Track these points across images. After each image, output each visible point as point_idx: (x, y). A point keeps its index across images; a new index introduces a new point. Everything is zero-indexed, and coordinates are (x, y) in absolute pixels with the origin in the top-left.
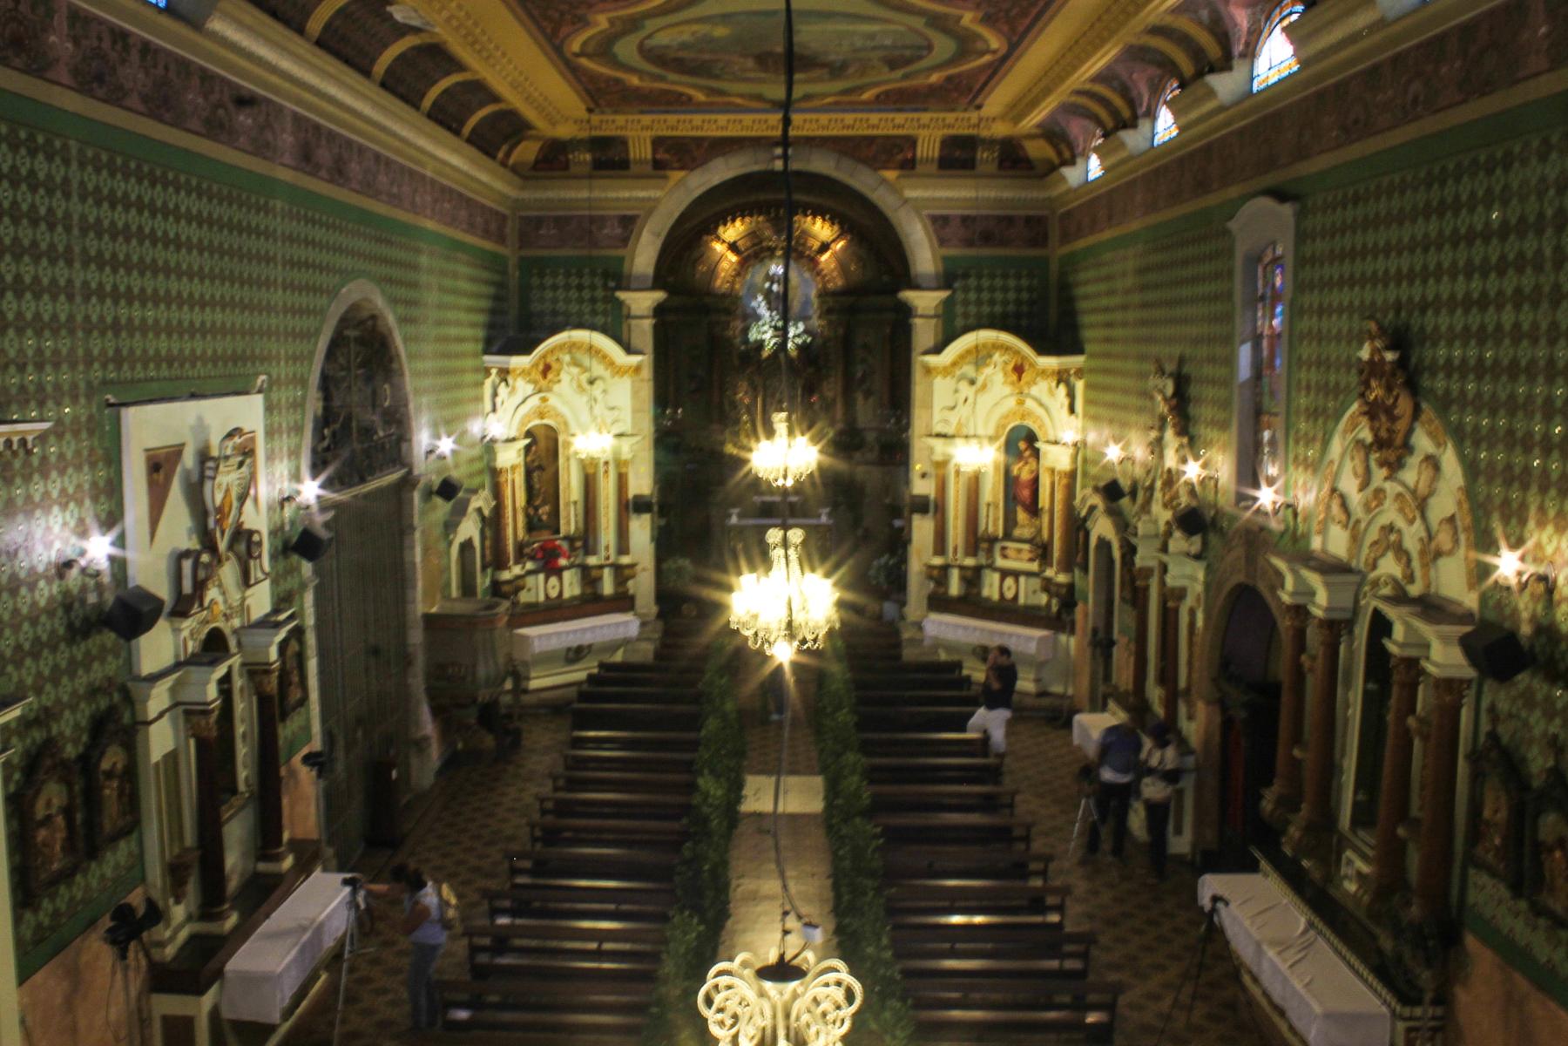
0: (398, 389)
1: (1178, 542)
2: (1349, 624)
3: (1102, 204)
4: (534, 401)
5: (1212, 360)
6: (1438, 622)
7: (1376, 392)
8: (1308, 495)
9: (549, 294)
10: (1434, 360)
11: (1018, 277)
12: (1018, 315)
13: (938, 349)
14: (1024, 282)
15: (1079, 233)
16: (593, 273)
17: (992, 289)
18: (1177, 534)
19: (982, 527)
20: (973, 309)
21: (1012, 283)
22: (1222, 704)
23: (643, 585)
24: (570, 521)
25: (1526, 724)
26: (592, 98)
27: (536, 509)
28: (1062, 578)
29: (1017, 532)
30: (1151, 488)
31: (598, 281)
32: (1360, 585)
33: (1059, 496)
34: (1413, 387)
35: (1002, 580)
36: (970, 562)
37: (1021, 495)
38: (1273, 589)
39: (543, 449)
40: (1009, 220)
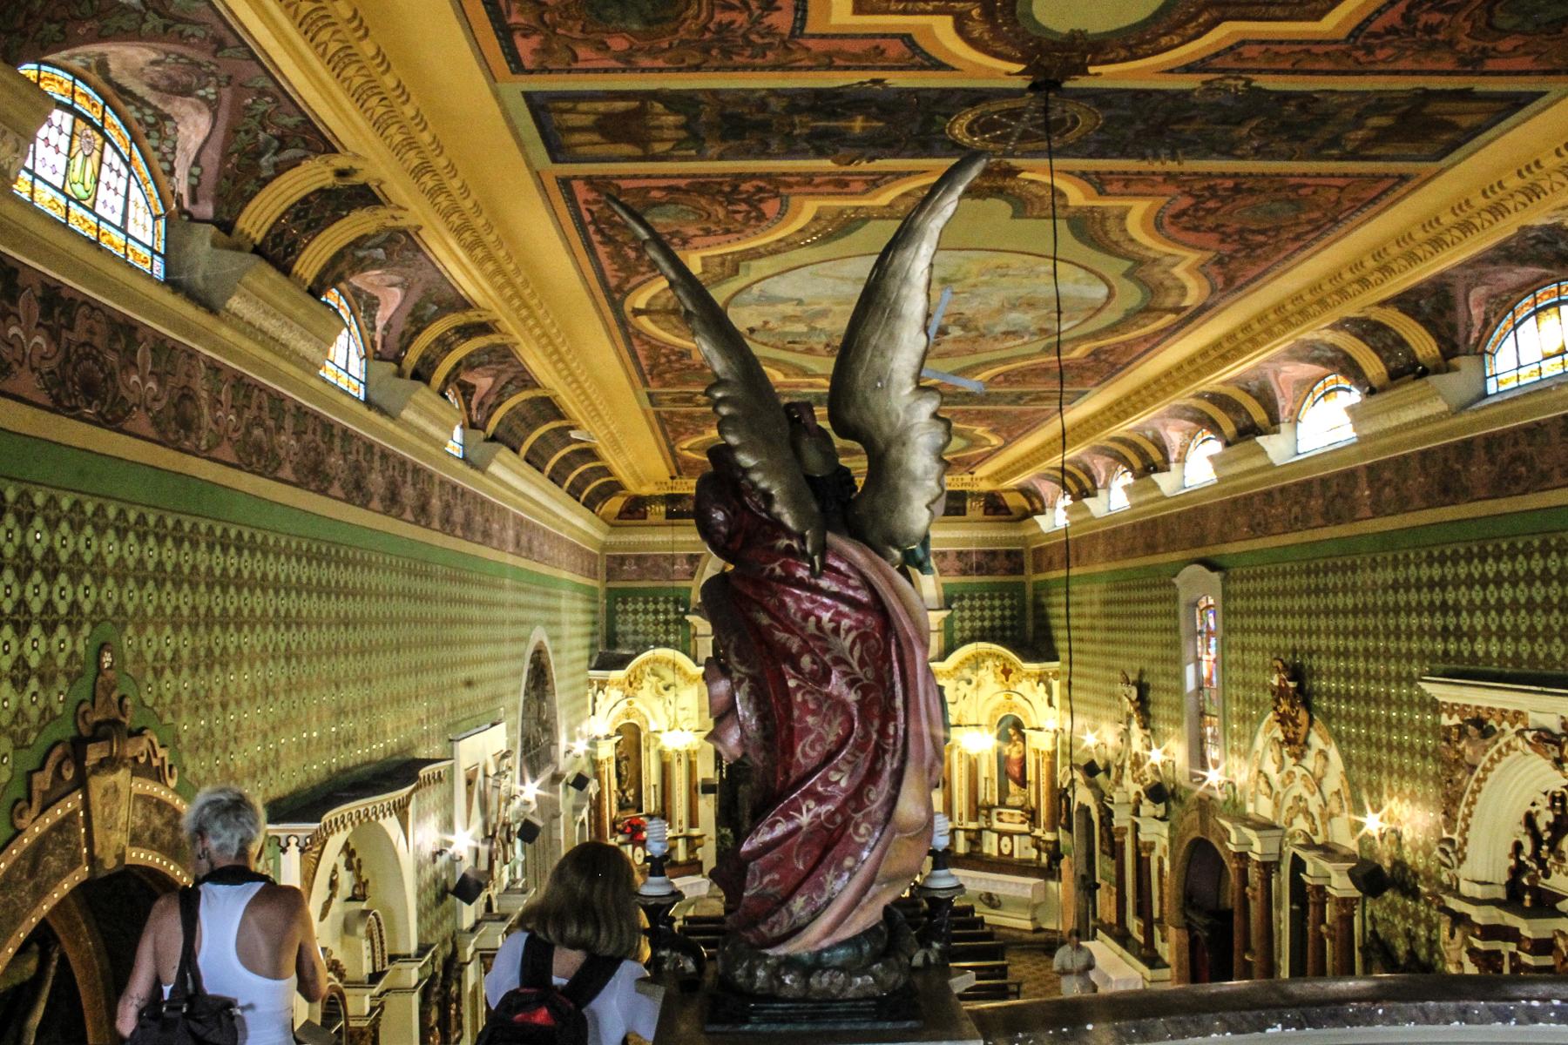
0: (551, 704)
1: (1147, 808)
2: (1277, 864)
3: (1068, 549)
4: (623, 705)
5: (1166, 674)
6: (1332, 860)
7: (1285, 707)
8: (1241, 772)
9: (631, 617)
10: (1319, 688)
11: (1002, 598)
12: (1003, 628)
13: (943, 656)
14: (1007, 602)
15: (1050, 566)
16: (666, 601)
17: (982, 609)
18: (1146, 802)
19: (981, 797)
20: (967, 624)
21: (997, 603)
22: (1189, 927)
23: (708, 855)
24: (651, 803)
25: (1394, 925)
26: (678, 469)
27: (624, 792)
28: (1049, 836)
29: (1009, 801)
30: (1122, 767)
31: (670, 607)
32: (1282, 837)
33: (1043, 771)
34: (1308, 707)
35: (1000, 839)
36: (973, 825)
37: (1013, 773)
38: (1221, 842)
39: (631, 740)
40: (993, 554)
